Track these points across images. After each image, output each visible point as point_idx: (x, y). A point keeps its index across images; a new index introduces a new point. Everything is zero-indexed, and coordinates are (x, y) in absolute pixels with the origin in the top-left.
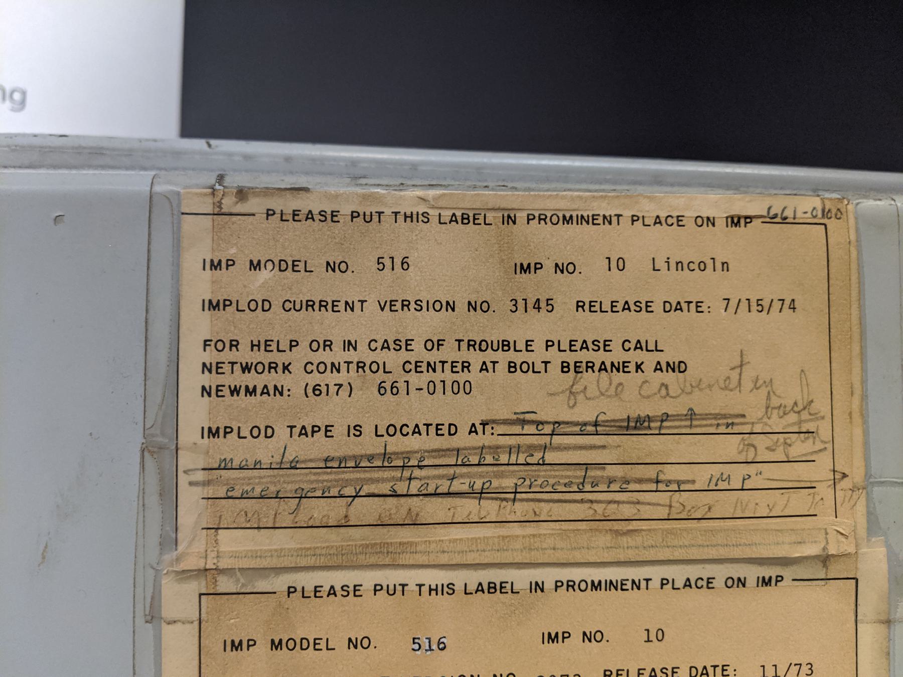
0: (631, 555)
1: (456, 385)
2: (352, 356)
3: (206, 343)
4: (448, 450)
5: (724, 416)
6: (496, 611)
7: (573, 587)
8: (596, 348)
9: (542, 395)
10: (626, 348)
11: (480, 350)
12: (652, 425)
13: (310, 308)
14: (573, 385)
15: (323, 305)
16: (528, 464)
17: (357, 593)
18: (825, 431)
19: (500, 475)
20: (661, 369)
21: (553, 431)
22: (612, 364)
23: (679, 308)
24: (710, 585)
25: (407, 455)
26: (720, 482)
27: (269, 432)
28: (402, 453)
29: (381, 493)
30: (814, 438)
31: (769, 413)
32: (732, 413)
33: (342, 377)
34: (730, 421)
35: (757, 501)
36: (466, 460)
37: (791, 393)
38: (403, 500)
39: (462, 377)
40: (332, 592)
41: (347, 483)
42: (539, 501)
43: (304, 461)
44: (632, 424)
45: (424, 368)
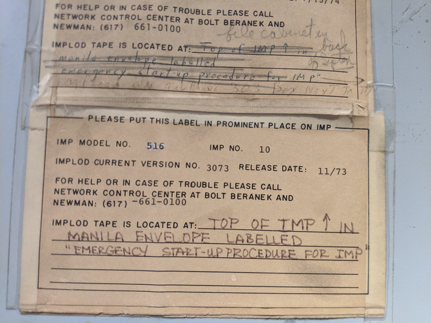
0: (254, 111)
1: (172, 28)
2: (124, 12)
3: (57, 5)
4: (168, 57)
5: (302, 48)
6: (189, 133)
7: (226, 124)
8: (248, 187)
9: (214, 35)
10: (263, 188)
11: (191, 186)
12: (267, 50)
13: (107, 164)
14: (229, 31)
15: (114, 162)
16: (206, 66)
17: (122, 121)
18: (353, 59)
19: (192, 71)
20: (272, 25)
21: (219, 51)
22: (249, 22)
23: (290, 169)
24: (293, 127)
25: (148, 58)
26: (299, 78)
27: (83, 45)
28: (145, 56)
29: (134, 74)
30: (348, 62)
31: (325, 48)
32: (306, 47)
33: (118, 22)
34: (305, 50)
35: (318, 88)
36: (176, 62)
37: (337, 40)
38: (144, 78)
39: (176, 24)
40: (110, 119)
41: (118, 68)
42: (211, 83)
43: (99, 58)
44: (257, 50)
45: (157, 18)
